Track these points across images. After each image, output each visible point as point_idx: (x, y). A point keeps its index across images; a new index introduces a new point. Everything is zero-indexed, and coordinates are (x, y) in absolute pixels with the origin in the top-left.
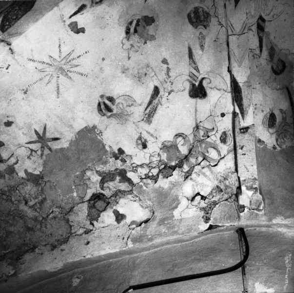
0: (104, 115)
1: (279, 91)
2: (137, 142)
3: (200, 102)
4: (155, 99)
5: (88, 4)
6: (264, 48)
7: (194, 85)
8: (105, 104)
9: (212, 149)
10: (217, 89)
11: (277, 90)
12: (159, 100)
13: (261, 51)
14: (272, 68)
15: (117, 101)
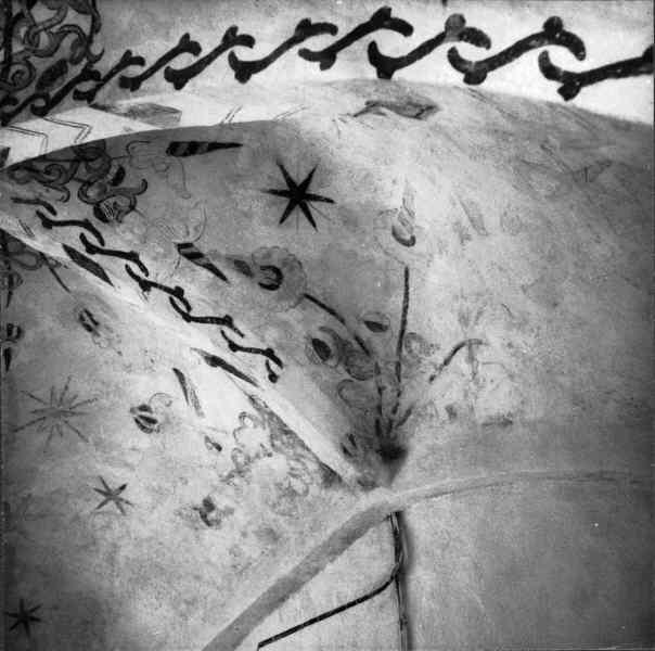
0: (151, 431)
1: (298, 307)
5: (6, 345)
6: (226, 273)
8: (142, 417)
11: (294, 307)
13: (224, 278)
14: (263, 286)
15: (153, 407)
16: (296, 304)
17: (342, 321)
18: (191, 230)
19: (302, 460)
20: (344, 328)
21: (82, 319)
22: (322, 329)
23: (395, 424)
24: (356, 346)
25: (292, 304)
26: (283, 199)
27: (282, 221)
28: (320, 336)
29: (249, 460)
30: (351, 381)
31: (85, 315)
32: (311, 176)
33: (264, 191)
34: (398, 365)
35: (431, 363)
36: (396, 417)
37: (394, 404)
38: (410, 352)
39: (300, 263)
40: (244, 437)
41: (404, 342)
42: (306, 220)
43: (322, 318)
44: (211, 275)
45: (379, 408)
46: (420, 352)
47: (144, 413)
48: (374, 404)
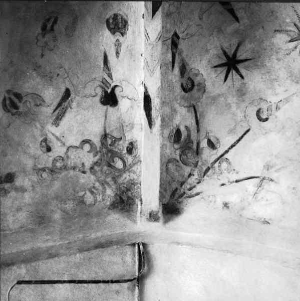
0: (9, 111)
2: (41, 144)
3: (111, 109)
4: (65, 101)
6: (176, 65)
7: (106, 92)
8: (10, 99)
9: (117, 158)
10: (128, 98)
12: (69, 103)
13: (173, 66)
14: (182, 86)
15: (25, 99)
16: (187, 107)
17: (198, 131)
18: (186, 33)
19: (106, 186)
20: (196, 134)
21: (48, 20)
22: (186, 127)
23: (185, 195)
24: (195, 147)
25: (186, 105)
26: (225, 58)
27: (215, 67)
28: (182, 129)
29: (65, 167)
30: (178, 161)
31: (53, 20)
32: (246, 60)
33: (222, 49)
34: (208, 169)
35: (228, 178)
36: (189, 193)
37: (193, 185)
38: (219, 166)
39: (205, 91)
40: (73, 154)
41: (219, 161)
42: (224, 75)
43: (191, 122)
44: (171, 60)
45: (182, 184)
46: (225, 170)
47: (16, 100)
48: (181, 180)
